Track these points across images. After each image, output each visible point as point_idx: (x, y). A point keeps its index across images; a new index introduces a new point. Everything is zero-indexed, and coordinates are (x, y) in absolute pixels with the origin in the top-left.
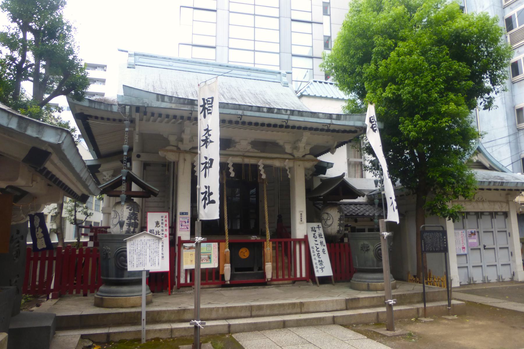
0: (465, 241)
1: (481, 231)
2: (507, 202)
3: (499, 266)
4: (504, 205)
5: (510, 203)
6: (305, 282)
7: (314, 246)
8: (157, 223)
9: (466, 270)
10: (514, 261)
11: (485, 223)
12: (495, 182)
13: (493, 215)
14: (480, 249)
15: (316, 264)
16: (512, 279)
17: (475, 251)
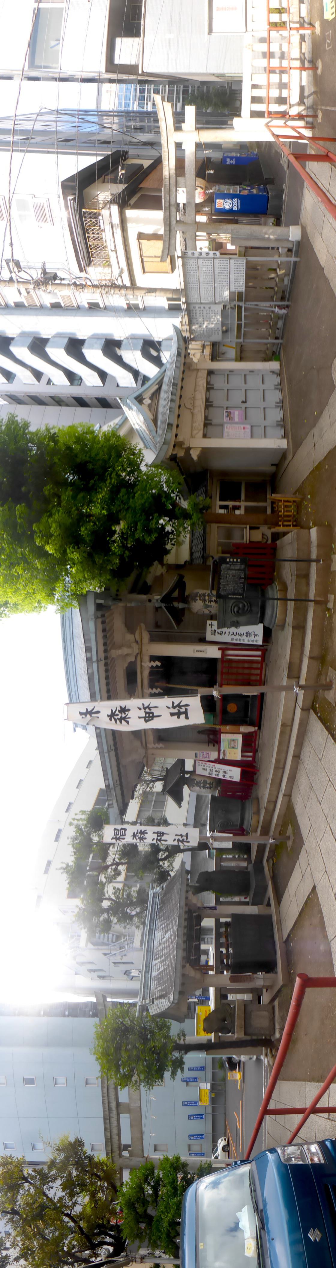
0: (237, 426)
1: (226, 404)
2: (198, 370)
3: (264, 387)
4: (200, 374)
5: (198, 367)
6: (267, 654)
7: (230, 637)
8: (204, 769)
9: (268, 429)
10: (259, 370)
11: (218, 398)
12: (172, 394)
13: (209, 388)
14: (246, 408)
15: (249, 641)
16: (278, 374)
17: (248, 414)
